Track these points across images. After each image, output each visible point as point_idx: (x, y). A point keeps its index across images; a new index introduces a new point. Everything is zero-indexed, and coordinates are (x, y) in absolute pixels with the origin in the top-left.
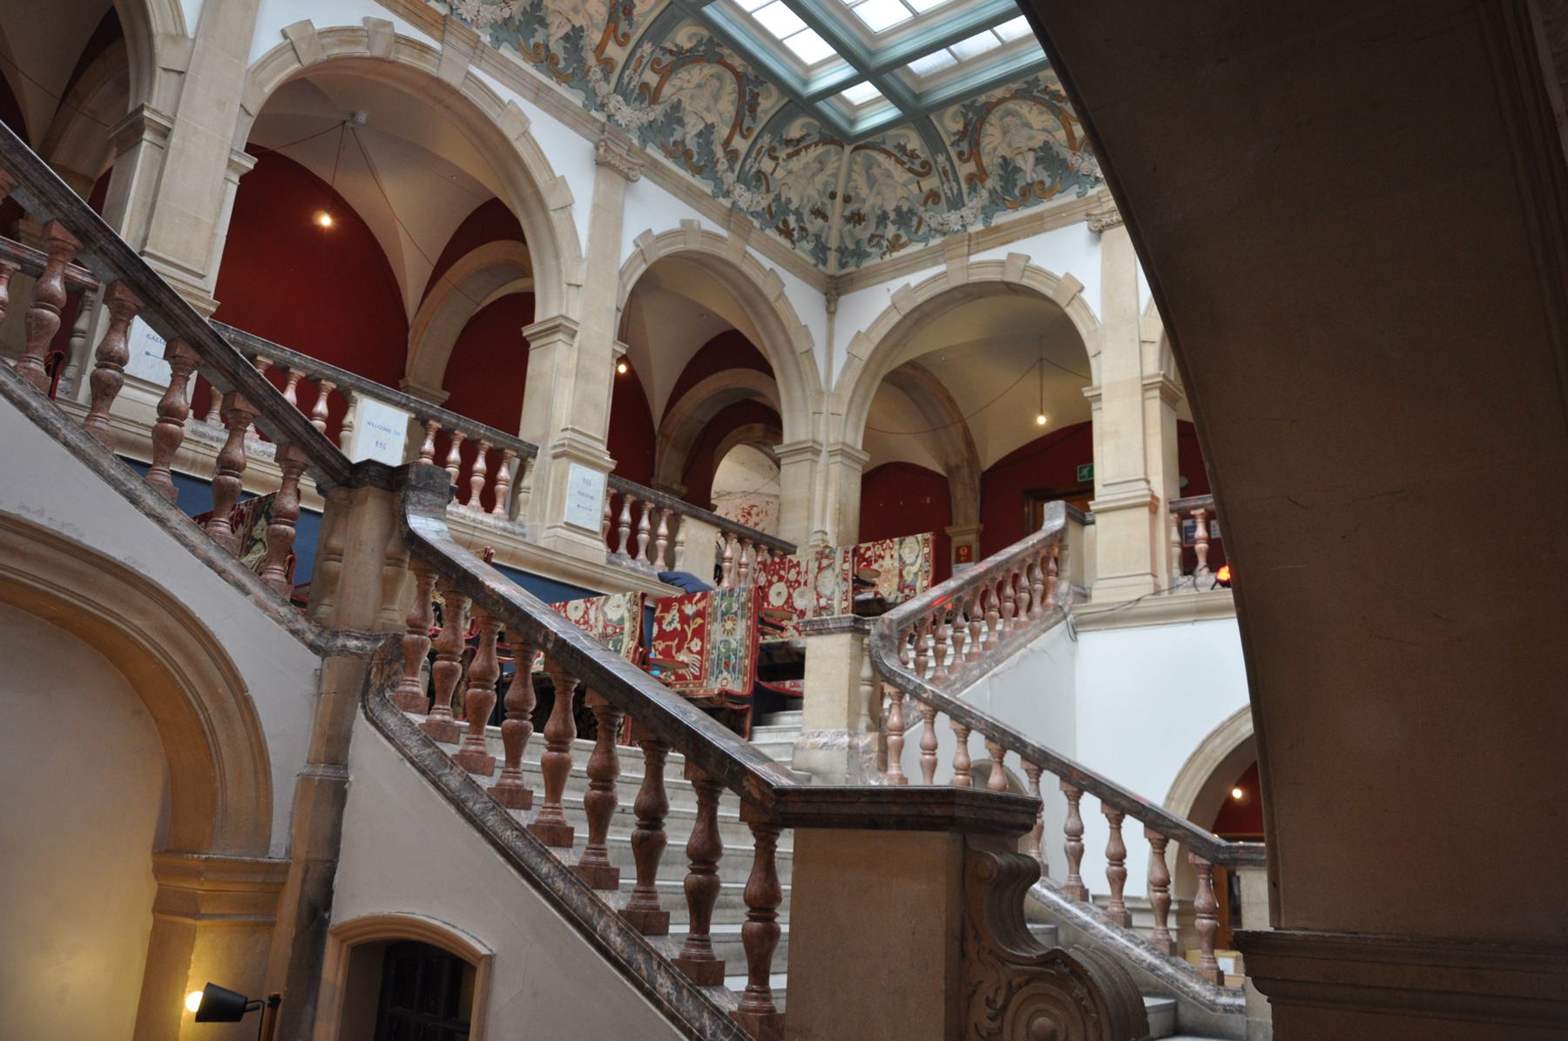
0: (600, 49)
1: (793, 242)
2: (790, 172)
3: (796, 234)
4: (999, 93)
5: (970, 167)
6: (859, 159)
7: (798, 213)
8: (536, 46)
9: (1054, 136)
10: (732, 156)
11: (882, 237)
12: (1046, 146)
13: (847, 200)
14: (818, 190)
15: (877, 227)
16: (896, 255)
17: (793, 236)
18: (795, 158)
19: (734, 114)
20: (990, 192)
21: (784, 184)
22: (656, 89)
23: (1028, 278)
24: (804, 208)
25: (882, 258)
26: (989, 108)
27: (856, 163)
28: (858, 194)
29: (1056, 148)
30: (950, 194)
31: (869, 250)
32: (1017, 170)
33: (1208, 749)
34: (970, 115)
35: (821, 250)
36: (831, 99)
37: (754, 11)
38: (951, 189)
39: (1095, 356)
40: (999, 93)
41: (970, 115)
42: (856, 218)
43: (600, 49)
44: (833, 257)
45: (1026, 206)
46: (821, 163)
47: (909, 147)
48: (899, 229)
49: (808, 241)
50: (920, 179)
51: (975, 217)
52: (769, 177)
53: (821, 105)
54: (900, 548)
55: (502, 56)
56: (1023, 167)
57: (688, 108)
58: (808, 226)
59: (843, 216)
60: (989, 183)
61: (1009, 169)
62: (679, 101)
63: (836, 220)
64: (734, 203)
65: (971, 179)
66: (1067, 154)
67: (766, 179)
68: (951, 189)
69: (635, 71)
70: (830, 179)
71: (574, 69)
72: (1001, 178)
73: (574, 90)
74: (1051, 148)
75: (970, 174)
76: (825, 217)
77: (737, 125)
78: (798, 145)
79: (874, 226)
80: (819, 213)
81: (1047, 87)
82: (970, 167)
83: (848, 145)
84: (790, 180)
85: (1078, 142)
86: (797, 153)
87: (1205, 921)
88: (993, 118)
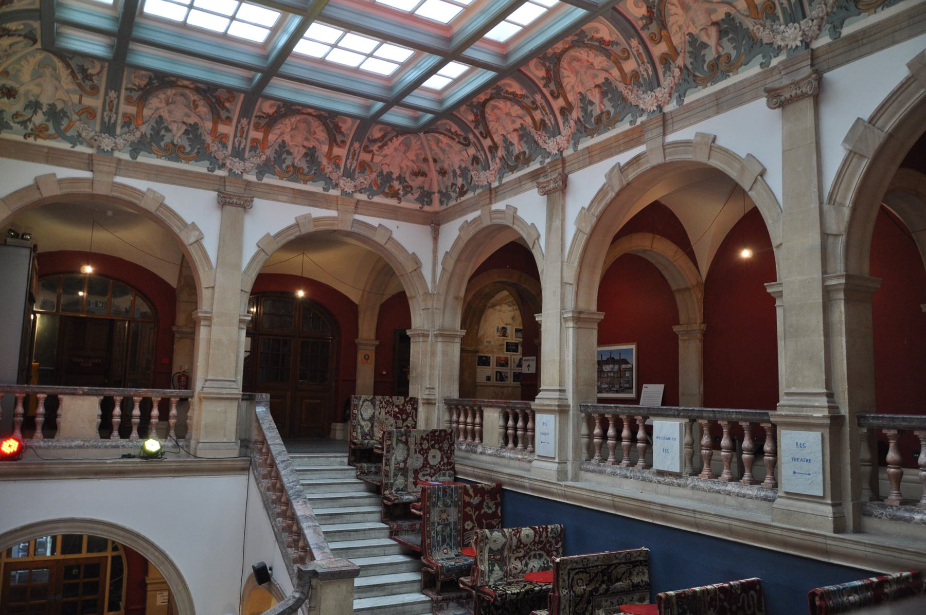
0: (214, 130)
1: (400, 199)
2: (386, 156)
3: (401, 192)
4: (560, 46)
5: (561, 102)
6: (430, 138)
7: (401, 179)
8: (167, 145)
9: (524, 121)
10: (335, 161)
11: (456, 185)
12: (523, 128)
13: (435, 161)
14: (412, 161)
15: (26, 107)
16: (463, 199)
17: (399, 194)
18: (385, 147)
19: (327, 137)
20: (500, 159)
21: (382, 164)
22: (263, 140)
23: (670, 154)
24: (405, 173)
25: (457, 201)
26: (558, 58)
27: (429, 140)
28: (439, 158)
29: (739, 18)
30: (107, 119)
31: (12, 124)
32: (704, 46)
33: (407, 607)
34: (547, 64)
35: (425, 197)
36: (416, 92)
37: (326, 56)
38: (646, 70)
39: (750, 190)
40: (560, 46)
41: (547, 64)
42: (443, 172)
43: (214, 130)
44: (436, 197)
45: (599, 134)
46: (406, 145)
47: (453, 130)
48: (48, 120)
49: (412, 194)
50: (466, 148)
51: (568, 143)
52: (371, 164)
53: (409, 100)
54: (374, 413)
55: (257, 101)
56: (594, 101)
57: (291, 144)
58: (411, 183)
59: (437, 171)
60: (680, 61)
61: (696, 46)
62: (284, 142)
63: (434, 175)
64: (343, 191)
65: (490, 148)
66: (621, 87)
67: (369, 165)
68: (646, 70)
69: (241, 137)
70: (418, 152)
71: (198, 149)
72: (153, 128)
73: (199, 163)
74: (733, 19)
75: (562, 107)
76: (424, 174)
77: (333, 141)
78: (383, 140)
79: (452, 177)
80: (421, 174)
81: (593, 36)
82: (561, 102)
83: (401, 136)
84: (387, 161)
85: (629, 77)
86: (386, 144)
87: (893, 470)
88: (564, 63)
